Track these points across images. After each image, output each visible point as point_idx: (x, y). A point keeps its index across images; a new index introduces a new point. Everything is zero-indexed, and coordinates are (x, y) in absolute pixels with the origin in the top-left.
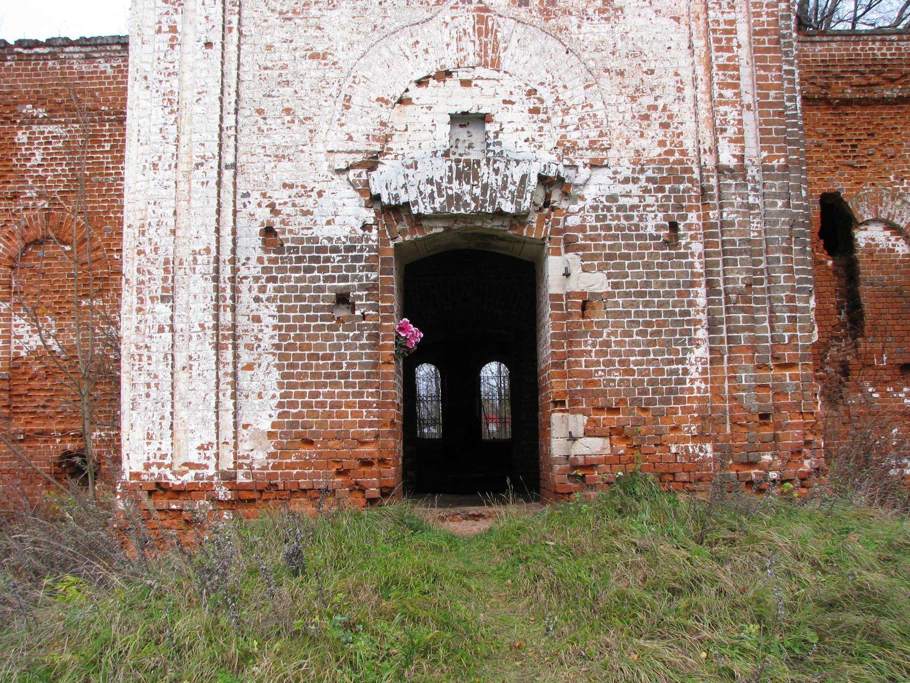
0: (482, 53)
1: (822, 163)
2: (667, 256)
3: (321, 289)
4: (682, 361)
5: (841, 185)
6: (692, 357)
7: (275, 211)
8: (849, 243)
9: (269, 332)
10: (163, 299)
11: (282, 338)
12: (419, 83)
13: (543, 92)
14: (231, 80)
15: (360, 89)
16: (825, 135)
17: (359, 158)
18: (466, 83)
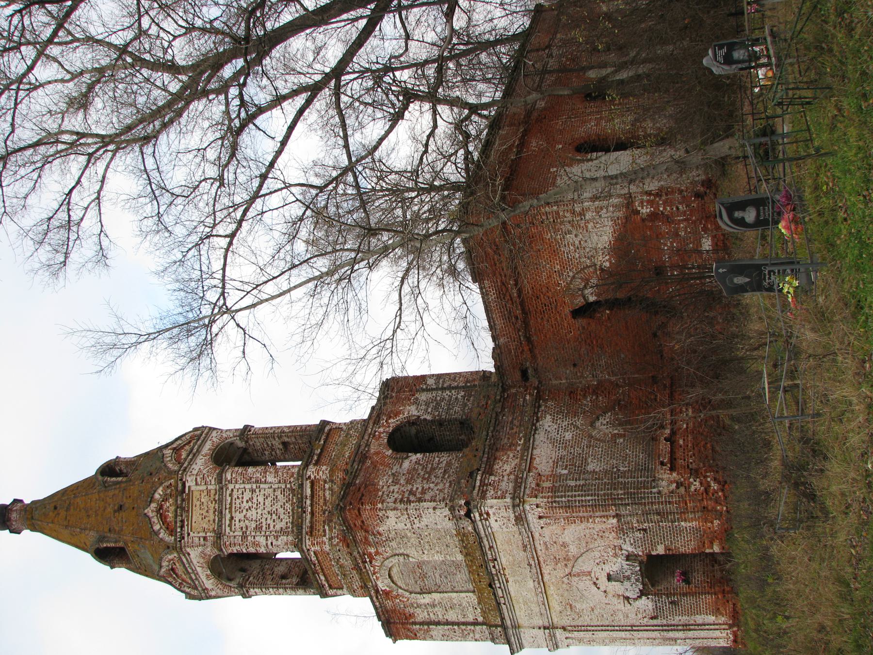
0: (587, 576)
1: (557, 318)
2: (650, 531)
3: (669, 608)
4: (686, 528)
5: (567, 311)
6: (684, 525)
7: (645, 617)
8: (596, 303)
9: (684, 617)
10: (676, 641)
11: (685, 615)
12: (598, 588)
13: (597, 561)
14: (604, 628)
15: (602, 601)
16: (542, 318)
17: (626, 602)
18: (597, 579)
